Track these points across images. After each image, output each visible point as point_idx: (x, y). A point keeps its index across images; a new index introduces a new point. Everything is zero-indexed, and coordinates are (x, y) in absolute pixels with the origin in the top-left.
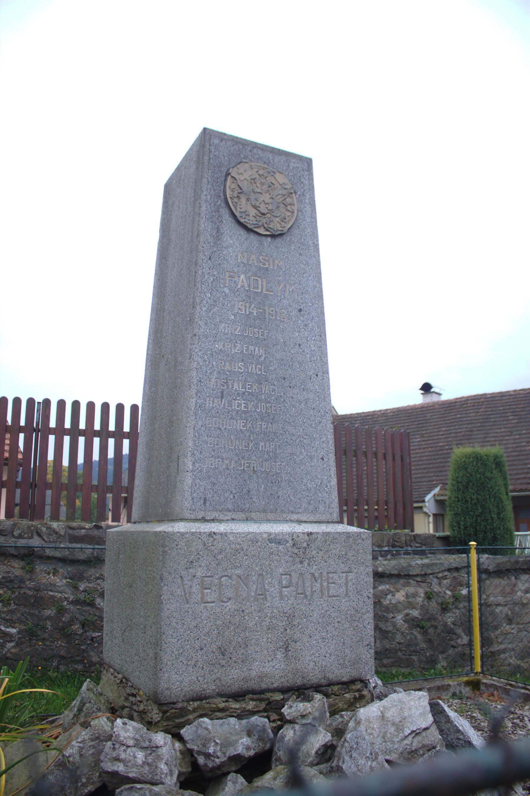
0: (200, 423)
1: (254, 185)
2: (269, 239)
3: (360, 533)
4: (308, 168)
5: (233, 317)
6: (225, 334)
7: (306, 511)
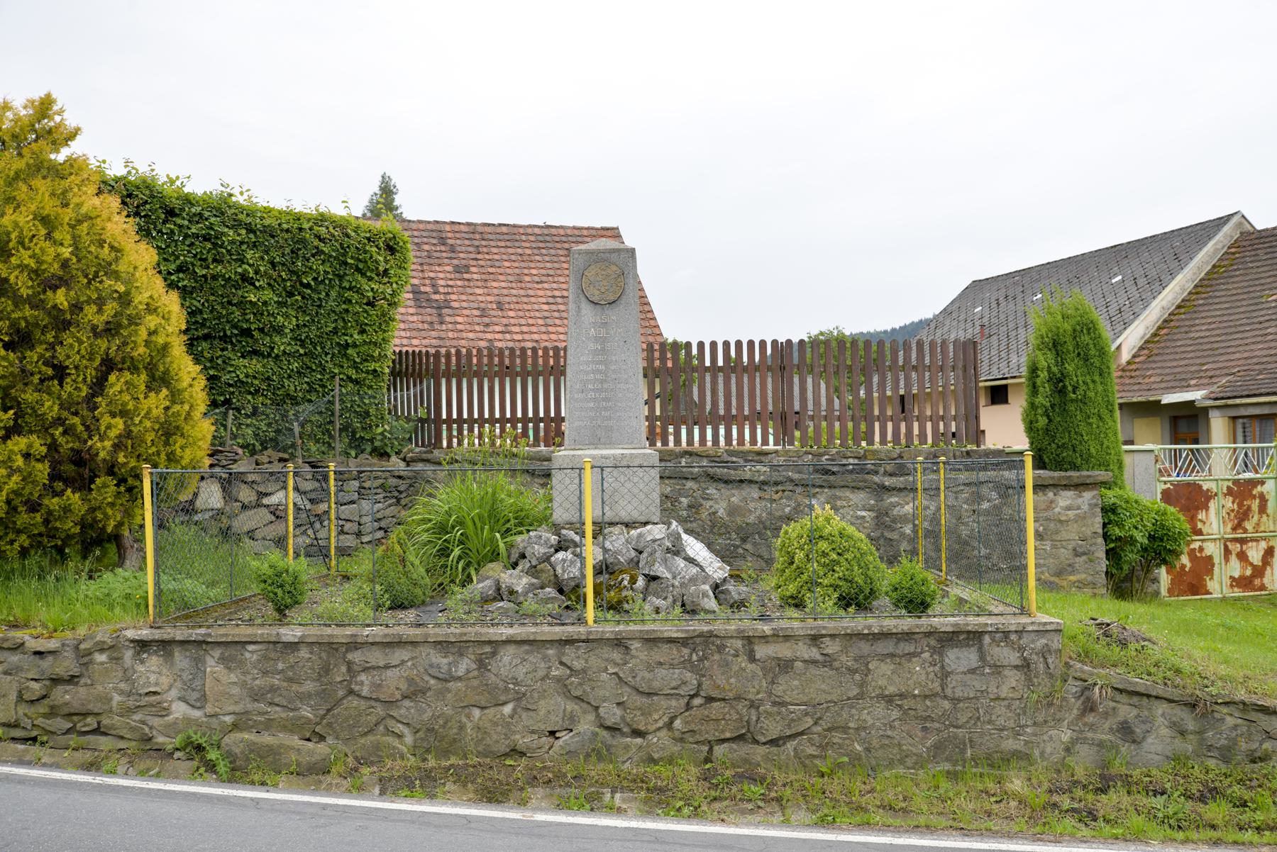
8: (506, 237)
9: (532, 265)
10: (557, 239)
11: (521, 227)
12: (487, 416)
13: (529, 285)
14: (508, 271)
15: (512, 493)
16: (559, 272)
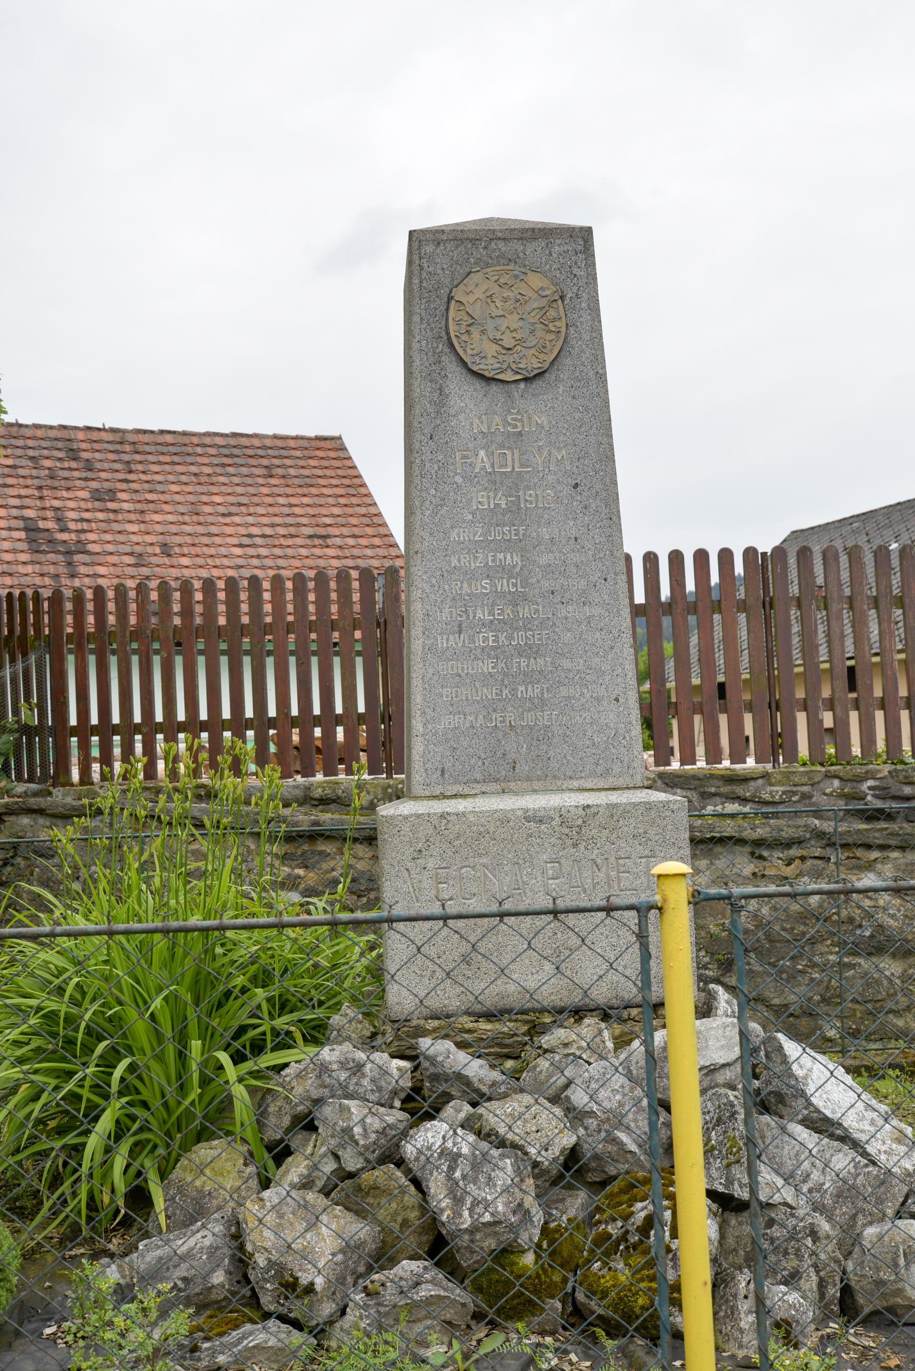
0: (431, 671)
1: (492, 305)
2: (522, 385)
3: (669, 802)
4: (585, 246)
5: (470, 517)
6: (460, 543)
7: (593, 774)
8: (172, 449)
9: (214, 489)
10: (250, 452)
11: (194, 434)
12: (159, 717)
13: (210, 519)
14: (178, 498)
15: (245, 902)
16: (256, 500)
